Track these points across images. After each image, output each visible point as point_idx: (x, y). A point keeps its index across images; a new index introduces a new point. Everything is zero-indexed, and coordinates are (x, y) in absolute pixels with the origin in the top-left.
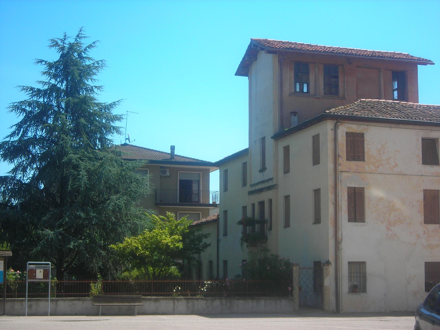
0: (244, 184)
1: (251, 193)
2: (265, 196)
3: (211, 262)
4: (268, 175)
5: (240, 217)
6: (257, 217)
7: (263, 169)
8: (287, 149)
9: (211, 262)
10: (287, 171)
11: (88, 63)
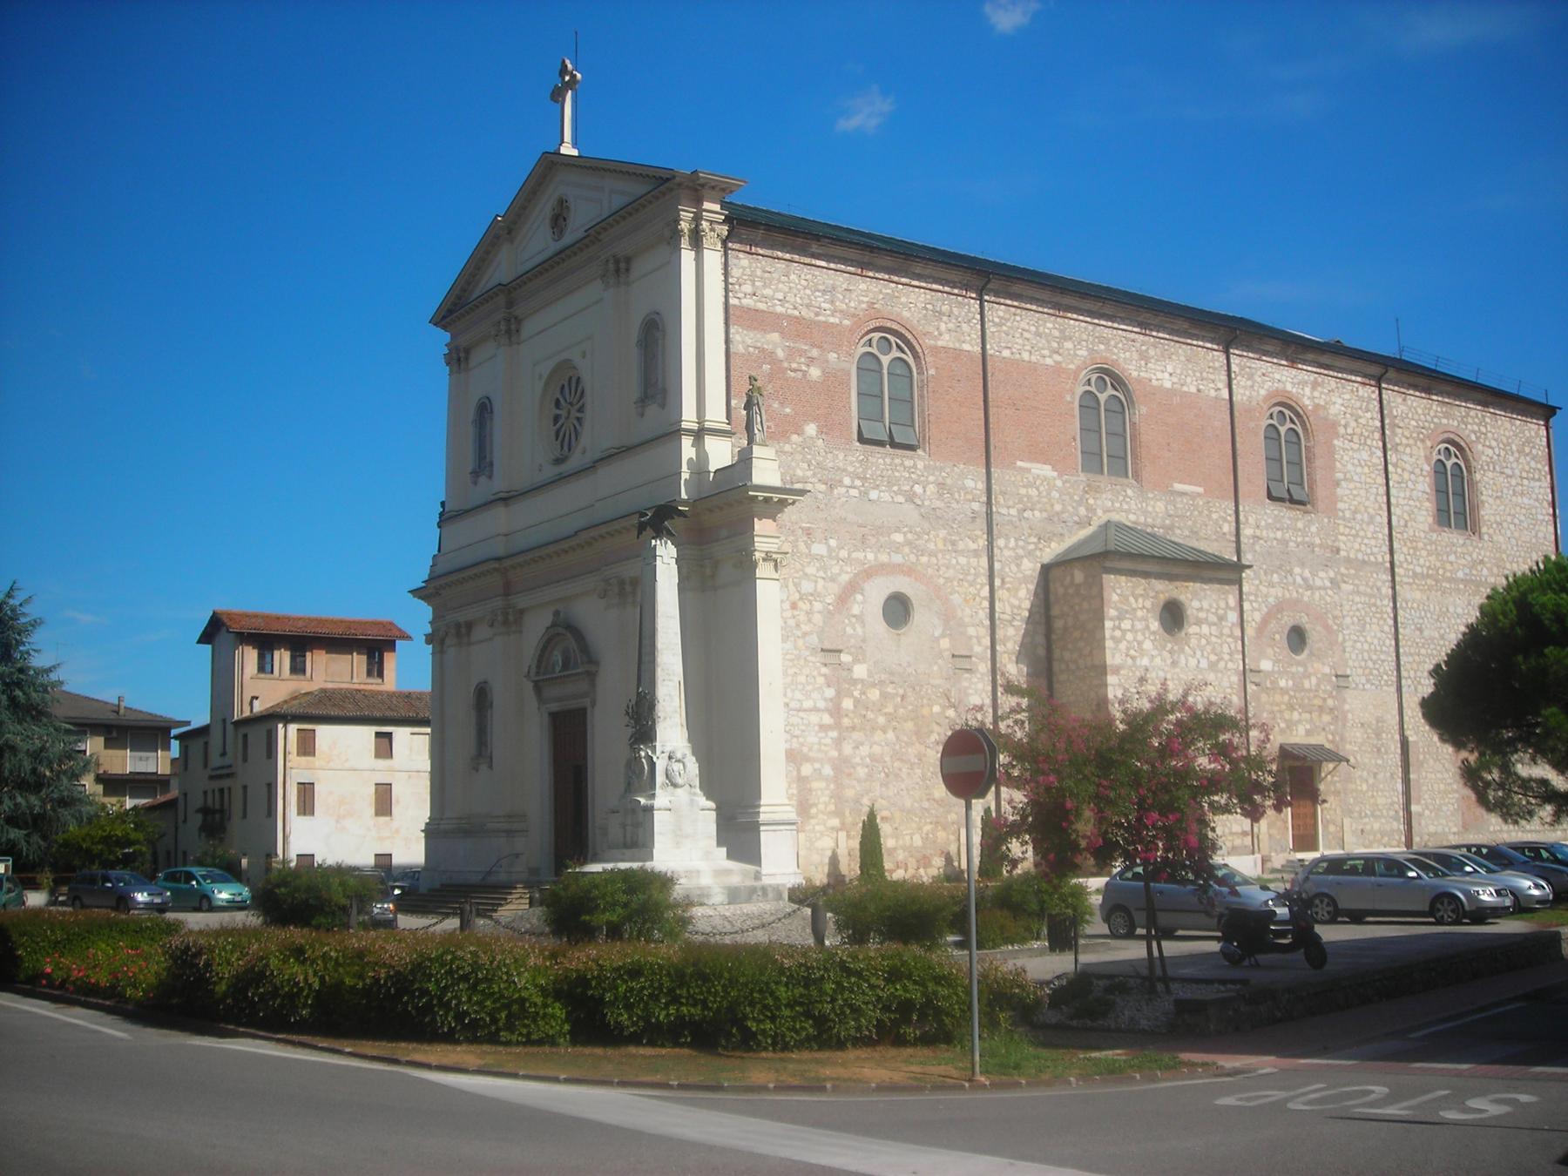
0: (206, 766)
1: (212, 778)
2: (225, 783)
3: (168, 853)
4: (227, 761)
5: (199, 803)
6: (217, 806)
7: (224, 754)
8: (245, 736)
9: (168, 853)
10: (245, 760)
11: (23, 620)
